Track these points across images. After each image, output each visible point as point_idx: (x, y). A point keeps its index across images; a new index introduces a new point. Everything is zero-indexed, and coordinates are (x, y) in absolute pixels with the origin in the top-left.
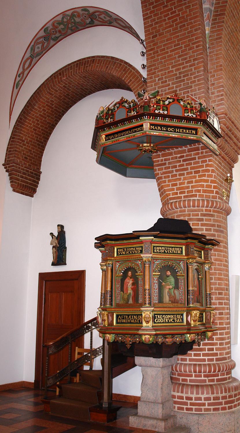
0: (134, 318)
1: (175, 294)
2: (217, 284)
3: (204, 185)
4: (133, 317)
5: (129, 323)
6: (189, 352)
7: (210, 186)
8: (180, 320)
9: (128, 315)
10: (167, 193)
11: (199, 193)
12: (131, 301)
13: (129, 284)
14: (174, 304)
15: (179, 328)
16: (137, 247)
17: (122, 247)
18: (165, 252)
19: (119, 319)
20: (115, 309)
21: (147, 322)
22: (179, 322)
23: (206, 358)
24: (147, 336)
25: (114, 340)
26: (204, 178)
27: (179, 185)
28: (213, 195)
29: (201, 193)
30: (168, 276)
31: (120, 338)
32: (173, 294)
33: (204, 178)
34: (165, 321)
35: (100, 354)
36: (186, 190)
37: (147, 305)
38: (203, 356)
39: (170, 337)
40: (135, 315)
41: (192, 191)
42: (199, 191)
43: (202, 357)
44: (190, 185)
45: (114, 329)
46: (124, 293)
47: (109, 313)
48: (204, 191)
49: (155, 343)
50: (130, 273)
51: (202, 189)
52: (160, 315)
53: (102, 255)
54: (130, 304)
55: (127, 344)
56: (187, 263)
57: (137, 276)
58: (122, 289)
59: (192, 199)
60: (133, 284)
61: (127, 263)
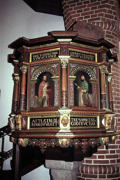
0: (48, 121)
1: (88, 98)
2: (116, 94)
3: (106, 10)
4: (48, 120)
5: (44, 127)
6: (93, 154)
7: (111, 12)
8: (93, 123)
9: (43, 119)
10: (73, 18)
11: (102, 17)
12: (46, 105)
13: (44, 88)
14: (88, 108)
15: (81, 132)
16: (53, 52)
17: (37, 53)
18: (79, 58)
19: (33, 123)
20: (29, 113)
21: (65, 124)
22: (93, 126)
23: (109, 160)
24: (65, 140)
25: (28, 144)
26: (107, 4)
27: (84, 11)
28: (112, 20)
29: (104, 17)
30: (82, 81)
31: (34, 143)
32: (87, 98)
33: (107, 4)
34: (80, 124)
35: (10, 156)
36: (90, 15)
37: (64, 107)
38: (106, 158)
39: (86, 141)
40: (50, 118)
41: (96, 15)
42: (102, 15)
43: (105, 159)
44: (94, 10)
45: (28, 133)
46: (38, 96)
47: (23, 117)
48: (107, 16)
49: (72, 146)
50: (45, 77)
51: (104, 13)
52: (75, 118)
53: (14, 81)
54: (45, 107)
55: (41, 148)
56: (100, 69)
57: (53, 80)
58: (37, 93)
59: (95, 21)
60: (48, 88)
61: (43, 67)
